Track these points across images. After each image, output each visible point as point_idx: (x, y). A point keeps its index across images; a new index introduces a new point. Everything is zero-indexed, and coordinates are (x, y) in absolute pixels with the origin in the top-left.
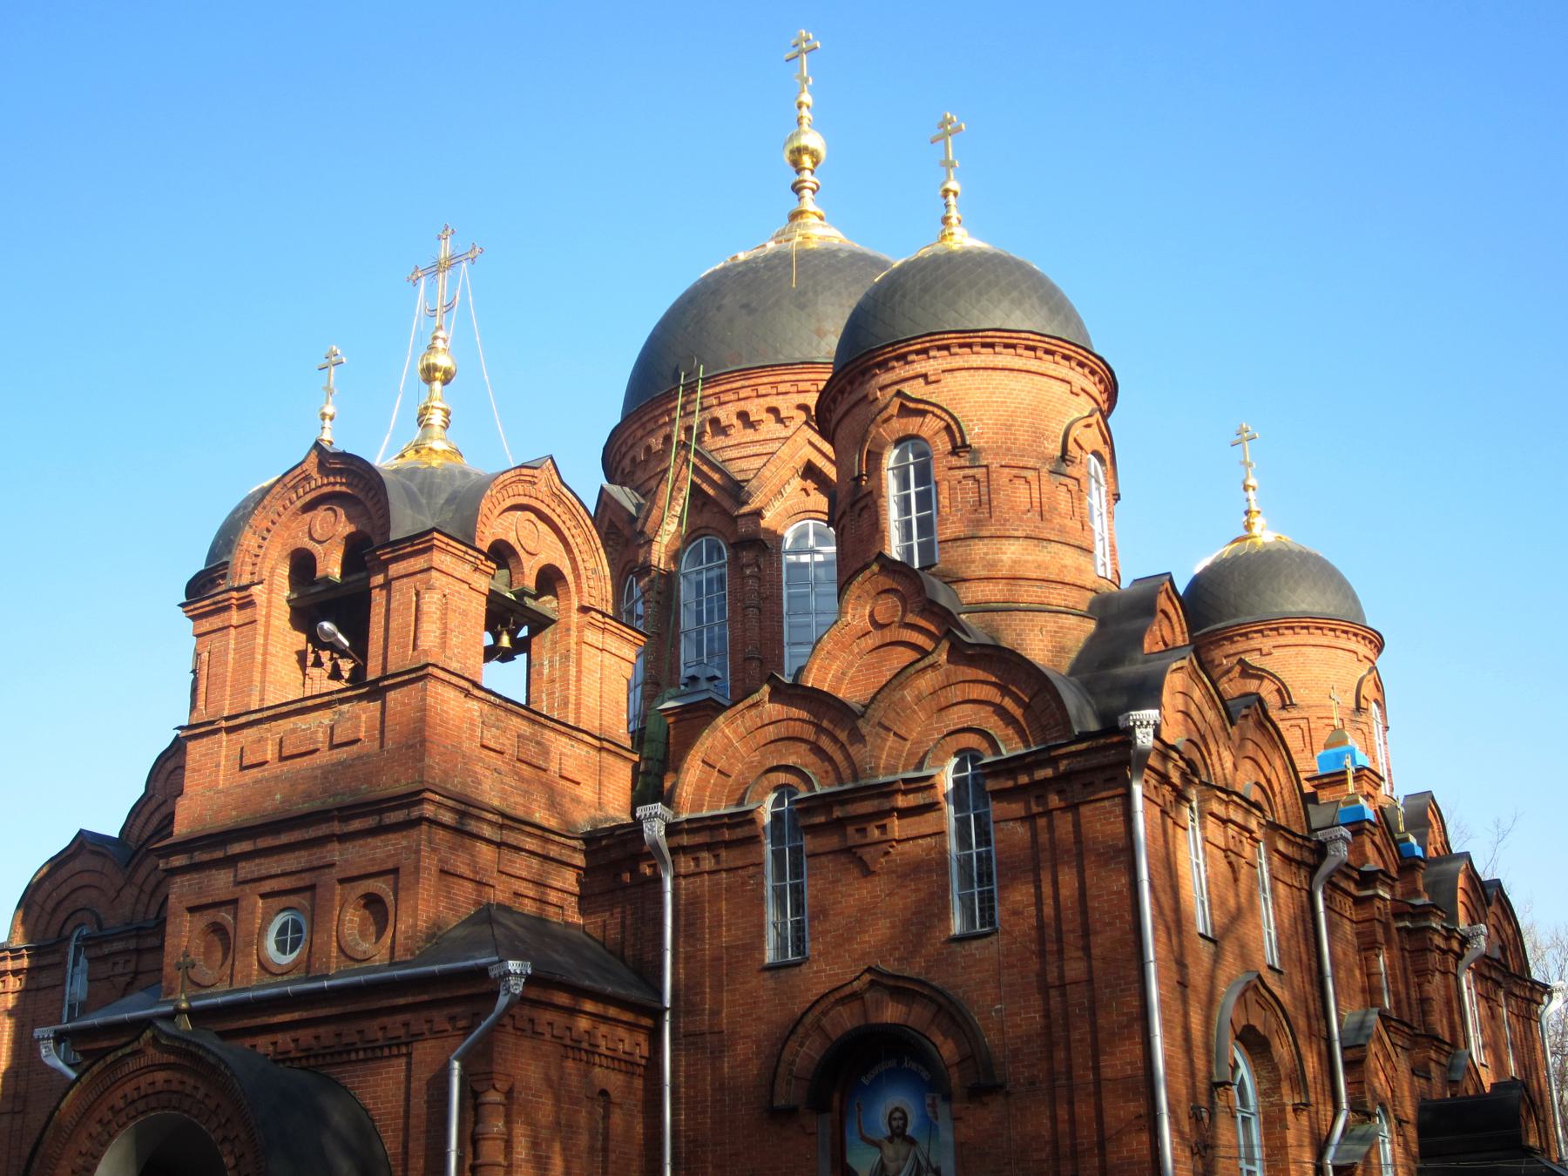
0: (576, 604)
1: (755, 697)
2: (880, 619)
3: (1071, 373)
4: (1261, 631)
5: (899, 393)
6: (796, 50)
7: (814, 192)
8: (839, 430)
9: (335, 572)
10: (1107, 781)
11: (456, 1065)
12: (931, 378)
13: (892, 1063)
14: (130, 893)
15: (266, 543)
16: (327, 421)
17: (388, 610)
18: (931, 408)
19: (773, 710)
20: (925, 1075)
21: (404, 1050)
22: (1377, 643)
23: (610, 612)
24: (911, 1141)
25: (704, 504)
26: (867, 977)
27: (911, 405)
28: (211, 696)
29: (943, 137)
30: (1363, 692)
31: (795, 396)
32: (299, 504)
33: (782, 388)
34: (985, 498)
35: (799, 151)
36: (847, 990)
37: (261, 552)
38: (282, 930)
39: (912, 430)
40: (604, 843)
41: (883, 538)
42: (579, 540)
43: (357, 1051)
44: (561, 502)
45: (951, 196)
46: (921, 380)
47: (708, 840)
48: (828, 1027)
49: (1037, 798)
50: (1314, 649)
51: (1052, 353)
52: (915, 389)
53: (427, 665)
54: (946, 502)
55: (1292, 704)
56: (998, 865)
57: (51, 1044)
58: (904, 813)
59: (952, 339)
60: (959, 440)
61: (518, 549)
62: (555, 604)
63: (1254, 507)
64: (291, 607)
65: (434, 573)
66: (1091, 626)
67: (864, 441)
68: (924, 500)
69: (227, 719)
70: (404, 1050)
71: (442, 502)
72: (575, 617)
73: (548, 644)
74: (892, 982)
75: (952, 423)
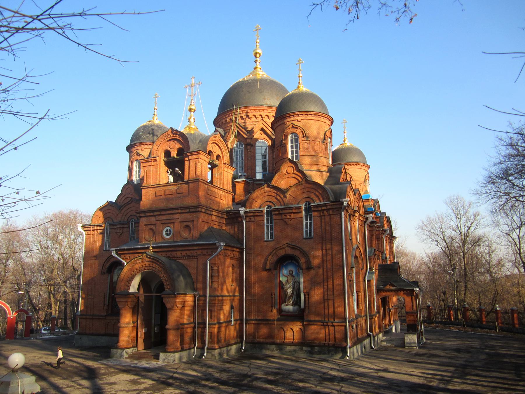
0: (222, 163)
1: (263, 187)
2: (289, 172)
3: (326, 121)
5: (292, 123)
6: (256, 29)
7: (259, 62)
8: (277, 128)
9: (175, 156)
10: (336, 211)
11: (208, 262)
12: (299, 121)
13: (290, 261)
14: (120, 215)
15: (159, 148)
16: (156, 110)
17: (189, 166)
18: (299, 127)
19: (266, 189)
20: (297, 264)
21: (196, 258)
22: (369, 167)
23: (229, 164)
24: (294, 276)
25: (239, 135)
26: (286, 245)
27: (295, 126)
28: (148, 180)
29: (299, 64)
30: (366, 178)
31: (259, 113)
32: (167, 140)
33: (256, 111)
34: (309, 147)
35: (256, 53)
36: (282, 247)
37: (158, 150)
38: (167, 231)
39: (294, 131)
40: (231, 214)
41: (288, 154)
42: (223, 149)
43: (185, 257)
45: (300, 77)
46: (297, 121)
47: (253, 215)
48: (278, 254)
49: (322, 212)
51: (323, 117)
52: (295, 123)
53: (199, 179)
54: (301, 148)
56: (314, 225)
57: (114, 252)
58: (294, 213)
59: (304, 113)
60: (304, 135)
61: (213, 152)
62: (218, 162)
63: (346, 137)
64: (164, 162)
65: (200, 159)
66: (328, 174)
67: (284, 132)
68: (296, 147)
69: (152, 185)
70: (196, 258)
71: (198, 142)
72: (223, 165)
73: (217, 171)
74: (291, 246)
75: (303, 131)
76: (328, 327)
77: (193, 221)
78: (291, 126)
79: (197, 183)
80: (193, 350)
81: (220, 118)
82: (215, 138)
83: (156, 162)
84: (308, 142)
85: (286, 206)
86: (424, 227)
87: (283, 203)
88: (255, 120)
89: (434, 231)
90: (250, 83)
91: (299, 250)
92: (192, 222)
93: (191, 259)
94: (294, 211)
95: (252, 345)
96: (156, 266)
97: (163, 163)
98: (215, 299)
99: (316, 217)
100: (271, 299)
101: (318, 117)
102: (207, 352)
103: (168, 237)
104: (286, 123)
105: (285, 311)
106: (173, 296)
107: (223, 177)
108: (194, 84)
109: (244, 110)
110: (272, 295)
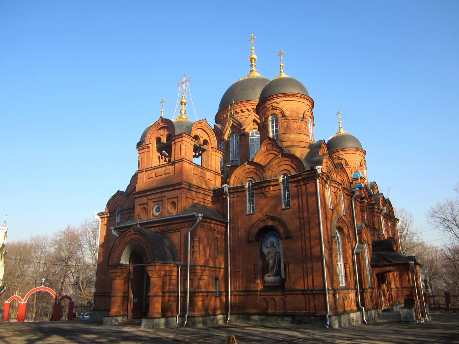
1: (245, 164)
4: (342, 151)
5: (272, 106)
7: (255, 66)
10: (312, 179)
11: (189, 233)
12: (278, 103)
13: (271, 233)
15: (152, 136)
16: (162, 113)
17: (175, 148)
19: (248, 166)
20: (277, 235)
22: (365, 153)
23: (217, 148)
24: (275, 247)
26: (266, 217)
27: (274, 108)
28: (142, 165)
29: (280, 55)
32: (158, 128)
33: (249, 105)
34: (288, 126)
35: (252, 59)
36: (262, 219)
38: (157, 209)
40: (216, 192)
42: (211, 135)
43: (171, 231)
44: (207, 127)
45: (282, 67)
46: (276, 103)
47: (236, 191)
50: (352, 154)
51: (301, 97)
52: (275, 105)
53: (183, 159)
54: (281, 127)
55: (348, 165)
59: (282, 95)
62: (206, 147)
63: (341, 127)
65: (184, 141)
67: (265, 115)
68: (277, 126)
69: (145, 169)
72: (210, 149)
73: (205, 154)
74: (271, 217)
75: (282, 111)
76: (307, 296)
77: (177, 197)
78: (271, 109)
79: (181, 162)
80: (176, 318)
81: (219, 116)
82: (201, 124)
83: (149, 149)
84: (287, 121)
85: (265, 180)
86: (435, 214)
87: (262, 178)
88: (248, 113)
89: (445, 217)
90: (244, 82)
91: (278, 220)
92: (177, 198)
93: (176, 232)
94: (272, 183)
95: (236, 316)
96: (139, 237)
97: (155, 149)
98: (194, 268)
99: (293, 188)
100: (254, 270)
101: (297, 98)
102: (188, 320)
103: (158, 214)
104: (266, 107)
105: (268, 282)
106: (153, 264)
107: (211, 159)
108: (185, 81)
109: (238, 105)
110: (255, 266)
